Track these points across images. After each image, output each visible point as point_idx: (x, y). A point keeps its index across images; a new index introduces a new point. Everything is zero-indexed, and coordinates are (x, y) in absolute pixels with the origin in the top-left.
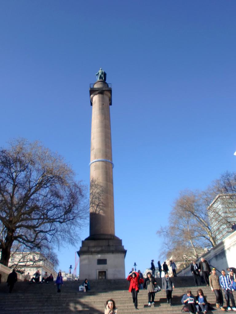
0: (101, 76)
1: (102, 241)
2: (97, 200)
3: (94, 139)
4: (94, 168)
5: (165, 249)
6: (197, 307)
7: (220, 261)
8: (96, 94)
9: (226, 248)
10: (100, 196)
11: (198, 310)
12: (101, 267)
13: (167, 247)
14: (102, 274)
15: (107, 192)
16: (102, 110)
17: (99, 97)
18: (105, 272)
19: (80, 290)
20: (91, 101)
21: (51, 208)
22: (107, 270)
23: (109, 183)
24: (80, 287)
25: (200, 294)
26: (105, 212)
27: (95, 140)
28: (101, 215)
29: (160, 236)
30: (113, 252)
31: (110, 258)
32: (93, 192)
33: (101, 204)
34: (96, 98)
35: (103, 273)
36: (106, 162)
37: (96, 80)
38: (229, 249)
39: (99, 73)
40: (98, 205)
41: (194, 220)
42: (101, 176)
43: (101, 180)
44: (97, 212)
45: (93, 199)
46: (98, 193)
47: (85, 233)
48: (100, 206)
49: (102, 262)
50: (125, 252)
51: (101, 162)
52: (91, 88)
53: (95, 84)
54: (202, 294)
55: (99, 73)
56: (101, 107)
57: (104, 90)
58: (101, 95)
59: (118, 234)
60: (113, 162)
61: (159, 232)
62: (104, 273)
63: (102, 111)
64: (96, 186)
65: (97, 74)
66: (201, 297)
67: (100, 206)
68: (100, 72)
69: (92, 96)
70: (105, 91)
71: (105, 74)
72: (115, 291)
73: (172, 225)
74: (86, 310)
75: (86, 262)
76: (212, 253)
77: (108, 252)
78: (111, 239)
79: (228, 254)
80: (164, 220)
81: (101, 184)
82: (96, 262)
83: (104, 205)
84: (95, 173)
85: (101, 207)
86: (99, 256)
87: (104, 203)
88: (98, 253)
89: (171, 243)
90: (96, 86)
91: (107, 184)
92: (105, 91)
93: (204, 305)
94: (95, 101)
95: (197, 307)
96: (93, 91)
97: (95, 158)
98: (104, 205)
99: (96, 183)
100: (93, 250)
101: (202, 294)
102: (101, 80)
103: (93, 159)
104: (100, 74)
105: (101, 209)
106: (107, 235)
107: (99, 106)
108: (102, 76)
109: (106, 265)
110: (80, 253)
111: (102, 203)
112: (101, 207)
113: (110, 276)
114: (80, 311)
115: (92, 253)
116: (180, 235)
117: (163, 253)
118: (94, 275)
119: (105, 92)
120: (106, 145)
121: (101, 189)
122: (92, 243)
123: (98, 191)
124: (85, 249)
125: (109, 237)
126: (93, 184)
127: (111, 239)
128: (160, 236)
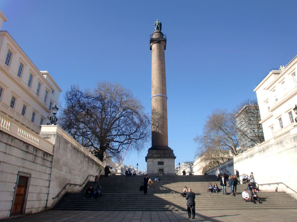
0: (158, 26)
1: (160, 150)
2: (157, 123)
3: (154, 79)
4: (154, 100)
5: (199, 152)
6: (214, 190)
7: (231, 168)
8: (155, 43)
9: (234, 162)
10: (159, 121)
11: (214, 191)
12: (160, 167)
13: (200, 150)
14: (161, 171)
15: (162, 119)
16: (159, 56)
17: (157, 45)
18: (163, 169)
19: (155, 180)
20: (150, 48)
21: (119, 121)
22: (164, 168)
23: (164, 112)
24: (155, 179)
25: (215, 184)
26: (162, 131)
27: (155, 80)
28: (160, 133)
29: (196, 142)
30: (167, 158)
31: (166, 161)
32: (154, 117)
33: (160, 126)
34: (154, 46)
35: (161, 170)
36: (162, 96)
37: (154, 29)
38: (235, 163)
39: (156, 24)
40: (158, 127)
41: (221, 133)
42: (159, 107)
43: (159, 110)
44: (157, 131)
45: (154, 122)
46: (158, 119)
47: (148, 145)
48: (159, 127)
49: (161, 163)
50: (175, 158)
51: (159, 97)
52: (151, 39)
53: (152, 35)
54: (216, 185)
55: (156, 24)
56: (158, 54)
57: (161, 40)
58: (158, 44)
59: (170, 146)
60: (168, 96)
61: (195, 140)
62: (162, 170)
63: (159, 58)
64: (156, 114)
65: (154, 24)
66: (216, 186)
67: (159, 127)
68: (157, 22)
69: (151, 44)
70: (161, 41)
71: (160, 24)
72: (173, 183)
73: (205, 135)
74: (85, 186)
75: (150, 163)
76: (227, 163)
77: (164, 157)
78: (166, 149)
79: (235, 165)
80: (200, 130)
81: (160, 113)
82: (157, 163)
83: (161, 127)
84: (155, 104)
85: (160, 128)
86: (159, 160)
87: (162, 125)
88: (158, 158)
89: (203, 148)
90: (154, 37)
91: (163, 112)
92: (161, 41)
93: (216, 189)
94: (154, 49)
95: (214, 190)
96: (152, 41)
97: (155, 93)
98: (161, 127)
99: (156, 111)
100: (155, 156)
101: (216, 185)
102: (158, 31)
103: (153, 94)
104: (157, 24)
105: (160, 130)
106: (164, 146)
107: (157, 53)
108: (159, 26)
109: (163, 165)
110: (146, 158)
111: (161, 125)
112: (160, 128)
113: (166, 172)
114: (165, 190)
115: (155, 158)
116: (211, 143)
117: (198, 155)
118: (156, 171)
119: (162, 42)
120: (162, 84)
121: (160, 116)
122: (154, 152)
123: (158, 117)
124: (150, 155)
125: (165, 148)
126: (153, 112)
127: (166, 149)
128: (196, 142)
